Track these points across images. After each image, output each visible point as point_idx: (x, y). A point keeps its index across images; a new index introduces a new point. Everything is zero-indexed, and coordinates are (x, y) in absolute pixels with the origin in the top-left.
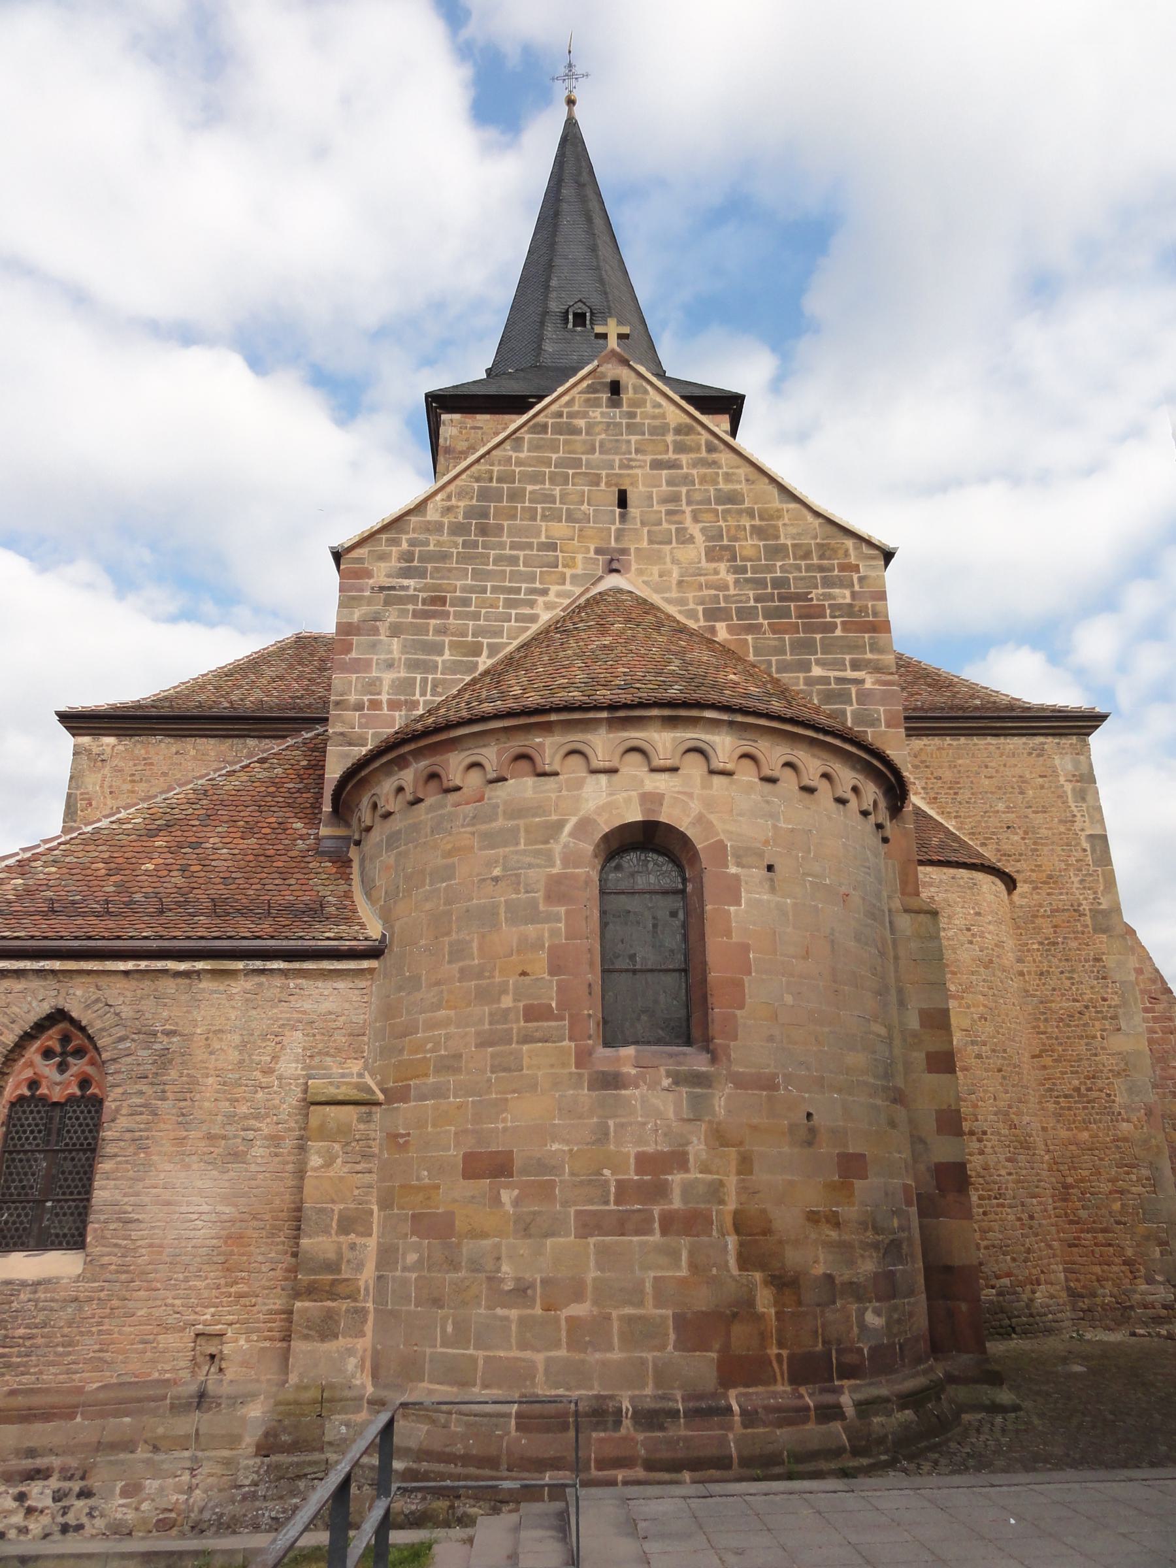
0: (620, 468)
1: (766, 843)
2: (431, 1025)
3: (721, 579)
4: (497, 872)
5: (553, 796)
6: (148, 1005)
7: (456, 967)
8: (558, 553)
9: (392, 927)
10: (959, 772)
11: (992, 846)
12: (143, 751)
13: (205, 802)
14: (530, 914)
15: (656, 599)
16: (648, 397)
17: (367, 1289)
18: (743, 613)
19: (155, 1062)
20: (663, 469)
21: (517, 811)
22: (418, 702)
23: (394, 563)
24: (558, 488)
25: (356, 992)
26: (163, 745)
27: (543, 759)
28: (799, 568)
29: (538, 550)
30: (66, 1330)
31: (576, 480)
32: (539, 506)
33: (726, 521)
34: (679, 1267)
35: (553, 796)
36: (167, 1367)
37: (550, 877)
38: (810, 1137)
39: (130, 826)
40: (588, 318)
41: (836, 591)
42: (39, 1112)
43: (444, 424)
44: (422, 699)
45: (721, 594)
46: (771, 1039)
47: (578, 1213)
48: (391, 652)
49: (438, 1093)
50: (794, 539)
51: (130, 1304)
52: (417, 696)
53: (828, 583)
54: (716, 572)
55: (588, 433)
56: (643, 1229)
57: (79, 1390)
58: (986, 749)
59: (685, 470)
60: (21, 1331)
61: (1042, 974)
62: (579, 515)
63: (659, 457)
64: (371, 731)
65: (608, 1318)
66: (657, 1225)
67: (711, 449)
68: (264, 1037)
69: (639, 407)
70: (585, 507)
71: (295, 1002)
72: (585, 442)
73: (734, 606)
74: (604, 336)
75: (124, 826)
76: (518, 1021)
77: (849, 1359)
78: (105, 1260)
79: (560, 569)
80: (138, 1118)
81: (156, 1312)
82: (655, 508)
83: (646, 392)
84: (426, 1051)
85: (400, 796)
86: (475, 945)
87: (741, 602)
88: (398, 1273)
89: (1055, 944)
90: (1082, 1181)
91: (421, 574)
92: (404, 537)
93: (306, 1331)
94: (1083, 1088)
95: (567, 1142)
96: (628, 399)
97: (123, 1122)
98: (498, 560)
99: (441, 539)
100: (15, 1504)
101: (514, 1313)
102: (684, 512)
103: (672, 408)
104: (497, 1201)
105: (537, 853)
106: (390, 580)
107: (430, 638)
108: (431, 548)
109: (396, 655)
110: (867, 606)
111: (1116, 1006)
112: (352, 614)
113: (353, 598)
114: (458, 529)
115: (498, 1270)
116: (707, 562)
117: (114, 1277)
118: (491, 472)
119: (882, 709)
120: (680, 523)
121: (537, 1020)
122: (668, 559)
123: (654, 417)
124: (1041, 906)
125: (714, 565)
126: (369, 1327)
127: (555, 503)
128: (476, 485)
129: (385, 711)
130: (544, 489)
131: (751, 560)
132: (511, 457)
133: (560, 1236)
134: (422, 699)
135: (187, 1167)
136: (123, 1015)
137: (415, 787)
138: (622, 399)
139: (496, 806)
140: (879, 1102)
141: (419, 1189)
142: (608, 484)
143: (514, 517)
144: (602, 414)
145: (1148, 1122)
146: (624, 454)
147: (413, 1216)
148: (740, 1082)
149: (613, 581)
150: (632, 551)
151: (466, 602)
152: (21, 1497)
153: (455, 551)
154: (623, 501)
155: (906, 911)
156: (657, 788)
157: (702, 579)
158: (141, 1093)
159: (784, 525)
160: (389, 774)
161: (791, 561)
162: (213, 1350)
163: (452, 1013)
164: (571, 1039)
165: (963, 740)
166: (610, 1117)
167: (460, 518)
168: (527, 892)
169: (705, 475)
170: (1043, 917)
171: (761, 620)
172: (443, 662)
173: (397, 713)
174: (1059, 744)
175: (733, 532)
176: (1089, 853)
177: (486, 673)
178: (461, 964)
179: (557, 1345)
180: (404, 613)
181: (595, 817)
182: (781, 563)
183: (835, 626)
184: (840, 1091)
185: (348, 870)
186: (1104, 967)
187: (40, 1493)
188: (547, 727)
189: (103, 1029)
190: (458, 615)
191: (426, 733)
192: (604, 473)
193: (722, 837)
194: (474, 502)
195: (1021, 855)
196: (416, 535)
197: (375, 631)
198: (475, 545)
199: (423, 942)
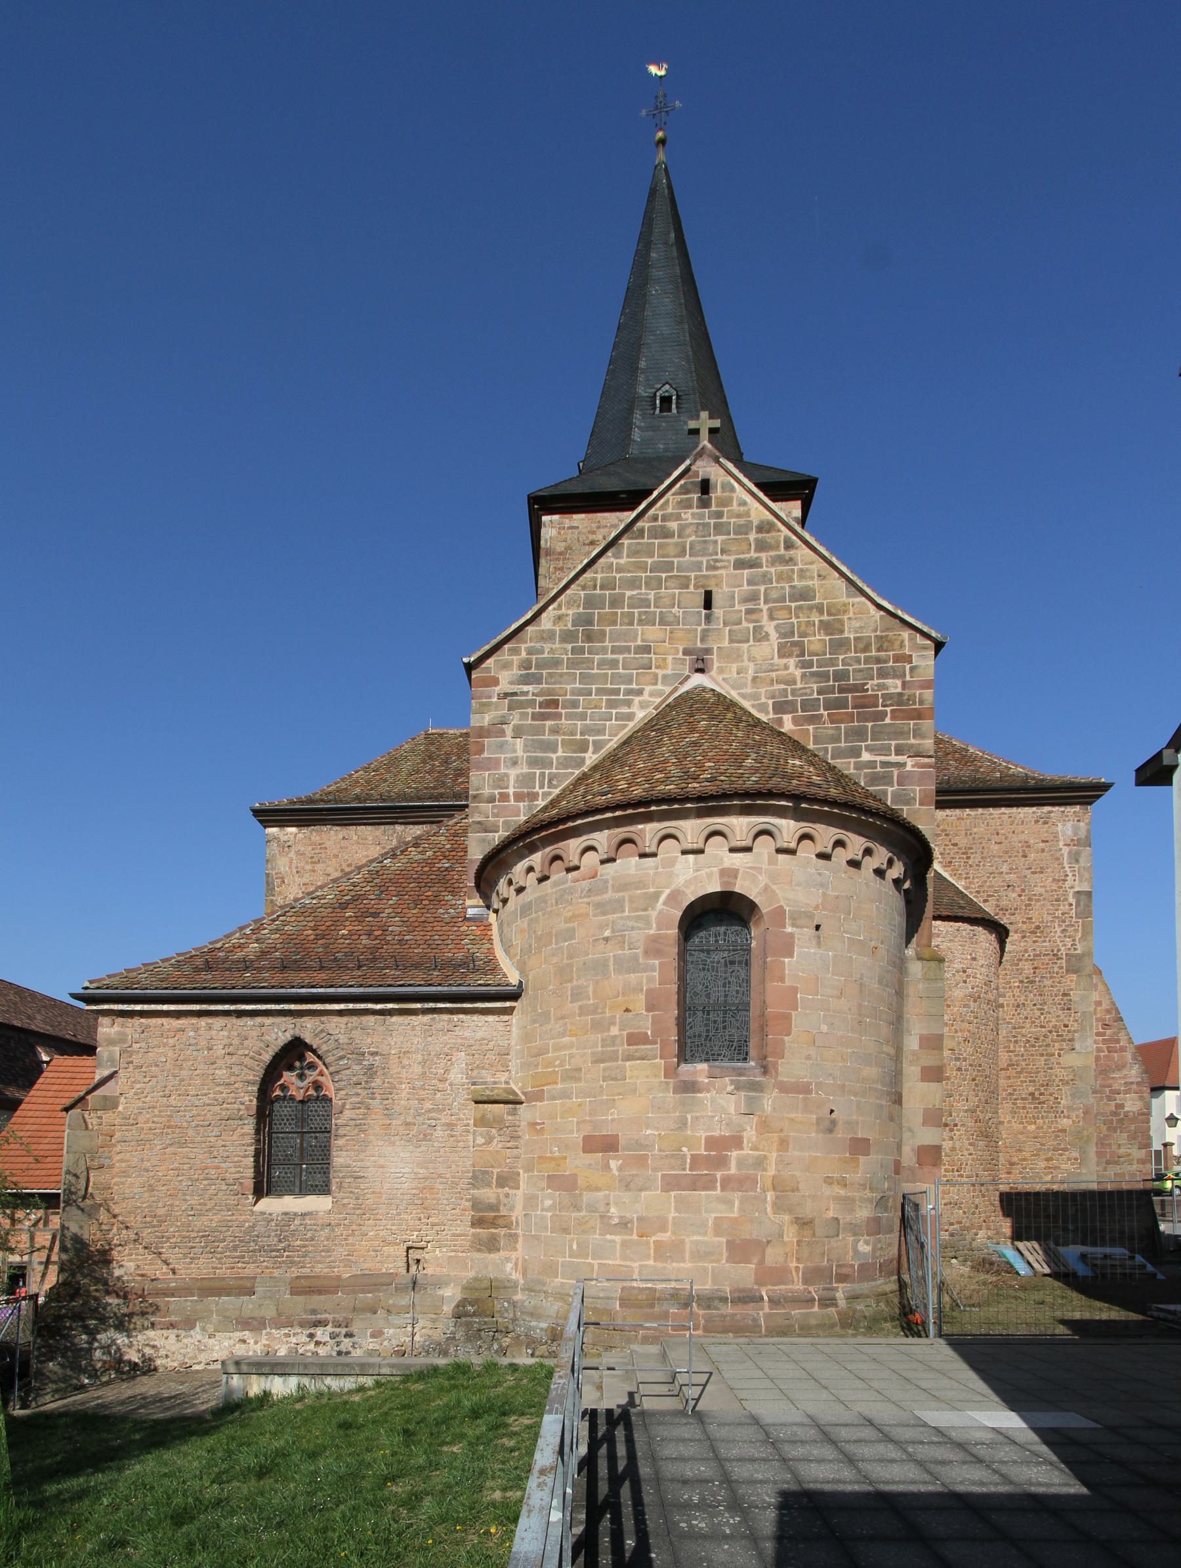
0: (707, 570)
1: (817, 907)
2: (558, 1048)
3: (790, 674)
4: (607, 933)
5: (651, 872)
6: (357, 1034)
7: (576, 1005)
8: (652, 655)
9: (527, 976)
10: (974, 838)
11: (992, 901)
12: (318, 838)
13: (378, 881)
14: (632, 966)
15: (734, 695)
16: (735, 495)
17: (517, 1222)
18: (805, 705)
19: (365, 1074)
20: (744, 569)
21: (623, 886)
22: (538, 793)
23: (516, 672)
24: (653, 592)
25: (502, 1024)
26: (332, 832)
27: (644, 841)
28: (858, 661)
29: (635, 654)
30: (326, 1243)
31: (668, 584)
32: (636, 611)
33: (798, 617)
34: (733, 1212)
35: (651, 872)
36: (390, 1266)
37: (648, 937)
38: (831, 1127)
39: (326, 901)
40: (674, 401)
41: (889, 682)
42: (290, 1107)
43: (545, 526)
44: (541, 791)
45: (789, 688)
46: (808, 1057)
47: (663, 1175)
48: (515, 751)
49: (565, 1095)
50: (856, 632)
51: (364, 1228)
52: (537, 789)
53: (883, 674)
54: (786, 667)
55: (679, 537)
56: (709, 1185)
57: (339, 1277)
58: (999, 818)
59: (765, 569)
60: (298, 1243)
61: (1018, 1006)
62: (670, 619)
63: (742, 556)
64: (501, 820)
65: (683, 1242)
66: (718, 1184)
67: (789, 545)
68: (438, 1056)
69: (725, 506)
70: (675, 610)
71: (458, 1032)
72: (676, 544)
73: (799, 699)
74: (695, 432)
75: (322, 901)
76: (623, 1045)
77: (844, 1271)
78: (345, 1201)
79: (653, 670)
80: (358, 1111)
81: (381, 1234)
82: (737, 607)
83: (733, 490)
84: (556, 1067)
85: (531, 874)
86: (591, 989)
87: (806, 694)
88: (538, 1213)
89: (1032, 982)
90: (1024, 1160)
91: (537, 680)
92: (523, 646)
93: (478, 1247)
94: (1037, 1093)
95: (657, 1129)
96: (716, 498)
97: (347, 1114)
98: (602, 664)
99: (554, 646)
100: (308, 1339)
101: (618, 1238)
102: (761, 610)
103: (757, 505)
104: (607, 1167)
105: (638, 918)
106: (513, 686)
107: (546, 737)
108: (546, 655)
109: (520, 753)
110: (914, 695)
111: (1075, 1031)
112: (483, 718)
113: (484, 705)
114: (568, 637)
115: (608, 1211)
116: (779, 658)
117: (352, 1211)
118: (595, 579)
119: (918, 789)
120: (757, 621)
121: (636, 1044)
122: (745, 657)
123: (739, 516)
124: (1026, 951)
125: (784, 661)
126: (519, 1246)
127: (650, 607)
128: (582, 593)
129: (512, 802)
130: (641, 594)
131: (817, 655)
132: (612, 563)
133: (651, 1190)
134: (541, 791)
135: (393, 1144)
136: (341, 1041)
137: (543, 865)
138: (711, 497)
139: (606, 881)
140: (884, 1103)
141: (552, 1159)
142: (696, 587)
143: (614, 623)
144: (693, 514)
145: (1084, 1118)
146: (711, 555)
147: (548, 1176)
148: (784, 1088)
149: (697, 680)
150: (715, 650)
151: (575, 704)
152: (311, 1336)
153: (565, 657)
154: (708, 604)
155: (920, 958)
156: (734, 864)
157: (774, 674)
158: (358, 1094)
159: (849, 619)
160: (522, 858)
161: (853, 654)
162: (418, 1257)
163: (574, 1039)
164: (661, 1058)
165: (980, 810)
166: (687, 1112)
167: (570, 625)
168: (630, 949)
169: (782, 572)
170: (1027, 960)
171: (822, 711)
172: (558, 758)
173: (522, 804)
174: (1063, 812)
175: (803, 628)
176: (1074, 907)
177: (595, 768)
178: (579, 1003)
179: (648, 1257)
180: (524, 716)
181: (684, 889)
182: (843, 657)
183: (884, 714)
184: (855, 1096)
185: (489, 933)
186: (1070, 1000)
187: (321, 1334)
188: (648, 818)
189: (328, 1051)
190: (569, 717)
191: (552, 823)
192: (693, 575)
193: (782, 903)
194: (581, 610)
195: (1016, 909)
196: (532, 644)
197: (502, 733)
198: (581, 650)
199: (551, 987)
